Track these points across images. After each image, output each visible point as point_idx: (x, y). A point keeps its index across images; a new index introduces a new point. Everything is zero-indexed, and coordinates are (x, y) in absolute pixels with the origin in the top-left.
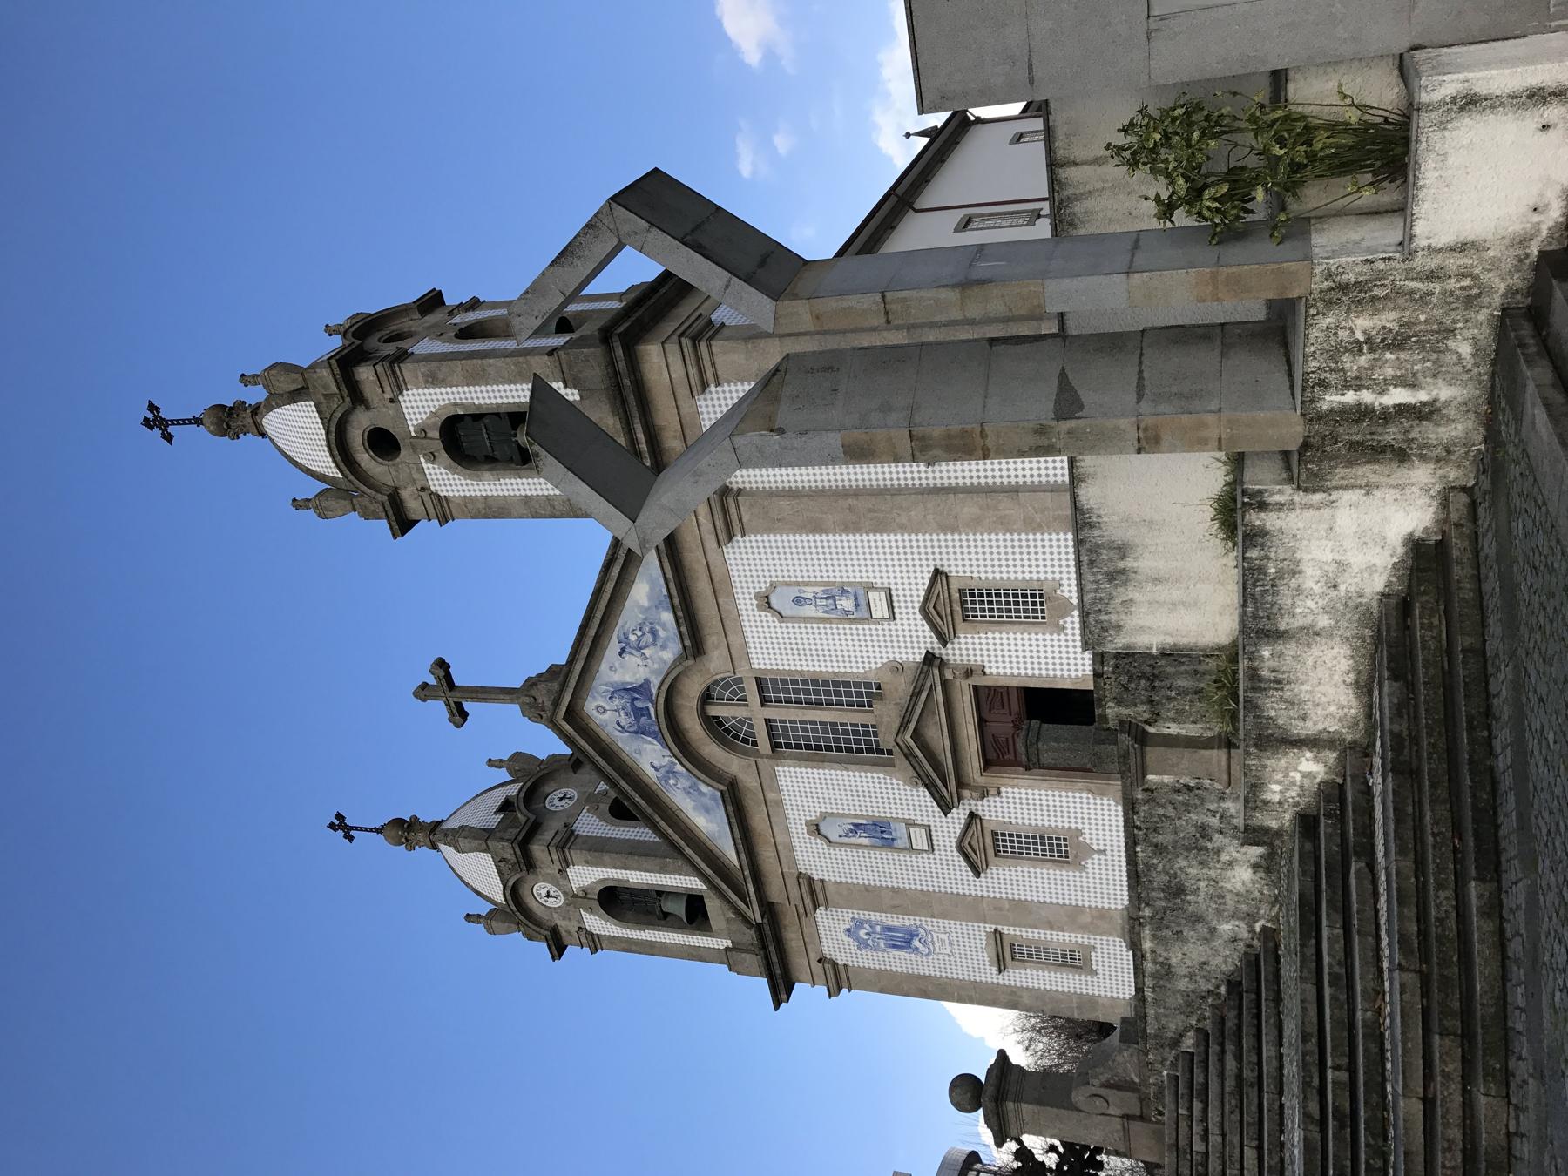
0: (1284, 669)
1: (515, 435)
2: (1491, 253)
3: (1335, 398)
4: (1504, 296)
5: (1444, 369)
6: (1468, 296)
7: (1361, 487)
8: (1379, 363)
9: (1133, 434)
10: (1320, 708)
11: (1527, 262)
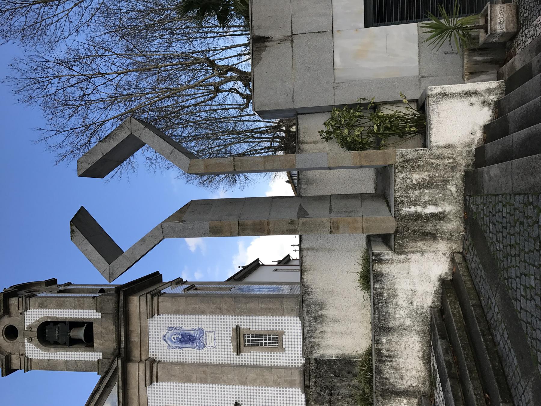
0: (392, 349)
1: (70, 332)
2: (459, 149)
3: (408, 210)
4: (465, 167)
5: (446, 198)
6: (453, 166)
7: (419, 252)
8: (423, 194)
9: (328, 225)
10: (408, 372)
11: (471, 153)
